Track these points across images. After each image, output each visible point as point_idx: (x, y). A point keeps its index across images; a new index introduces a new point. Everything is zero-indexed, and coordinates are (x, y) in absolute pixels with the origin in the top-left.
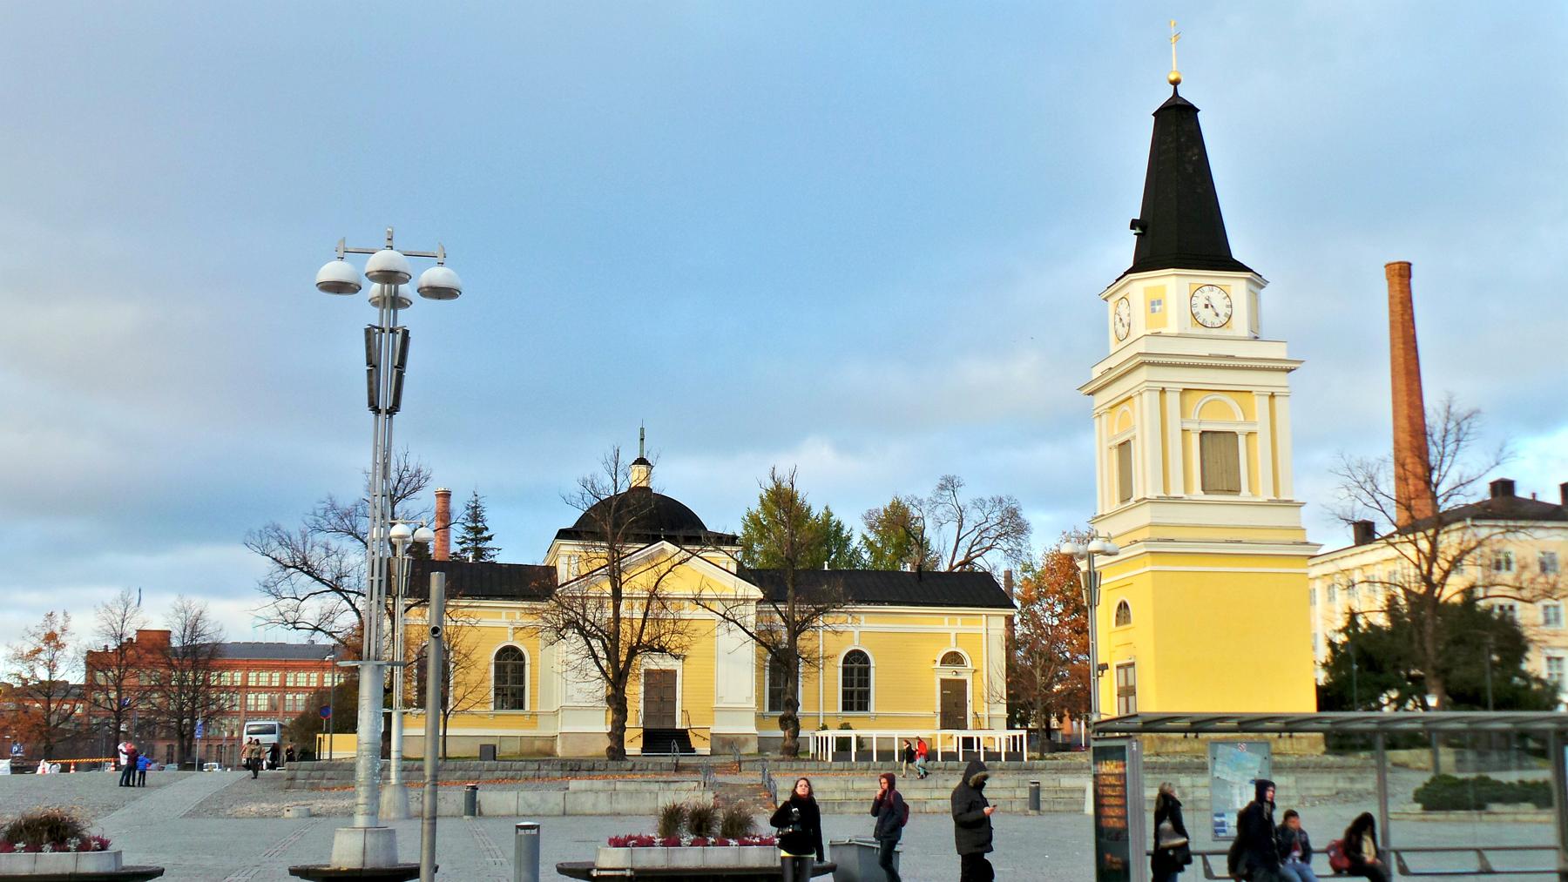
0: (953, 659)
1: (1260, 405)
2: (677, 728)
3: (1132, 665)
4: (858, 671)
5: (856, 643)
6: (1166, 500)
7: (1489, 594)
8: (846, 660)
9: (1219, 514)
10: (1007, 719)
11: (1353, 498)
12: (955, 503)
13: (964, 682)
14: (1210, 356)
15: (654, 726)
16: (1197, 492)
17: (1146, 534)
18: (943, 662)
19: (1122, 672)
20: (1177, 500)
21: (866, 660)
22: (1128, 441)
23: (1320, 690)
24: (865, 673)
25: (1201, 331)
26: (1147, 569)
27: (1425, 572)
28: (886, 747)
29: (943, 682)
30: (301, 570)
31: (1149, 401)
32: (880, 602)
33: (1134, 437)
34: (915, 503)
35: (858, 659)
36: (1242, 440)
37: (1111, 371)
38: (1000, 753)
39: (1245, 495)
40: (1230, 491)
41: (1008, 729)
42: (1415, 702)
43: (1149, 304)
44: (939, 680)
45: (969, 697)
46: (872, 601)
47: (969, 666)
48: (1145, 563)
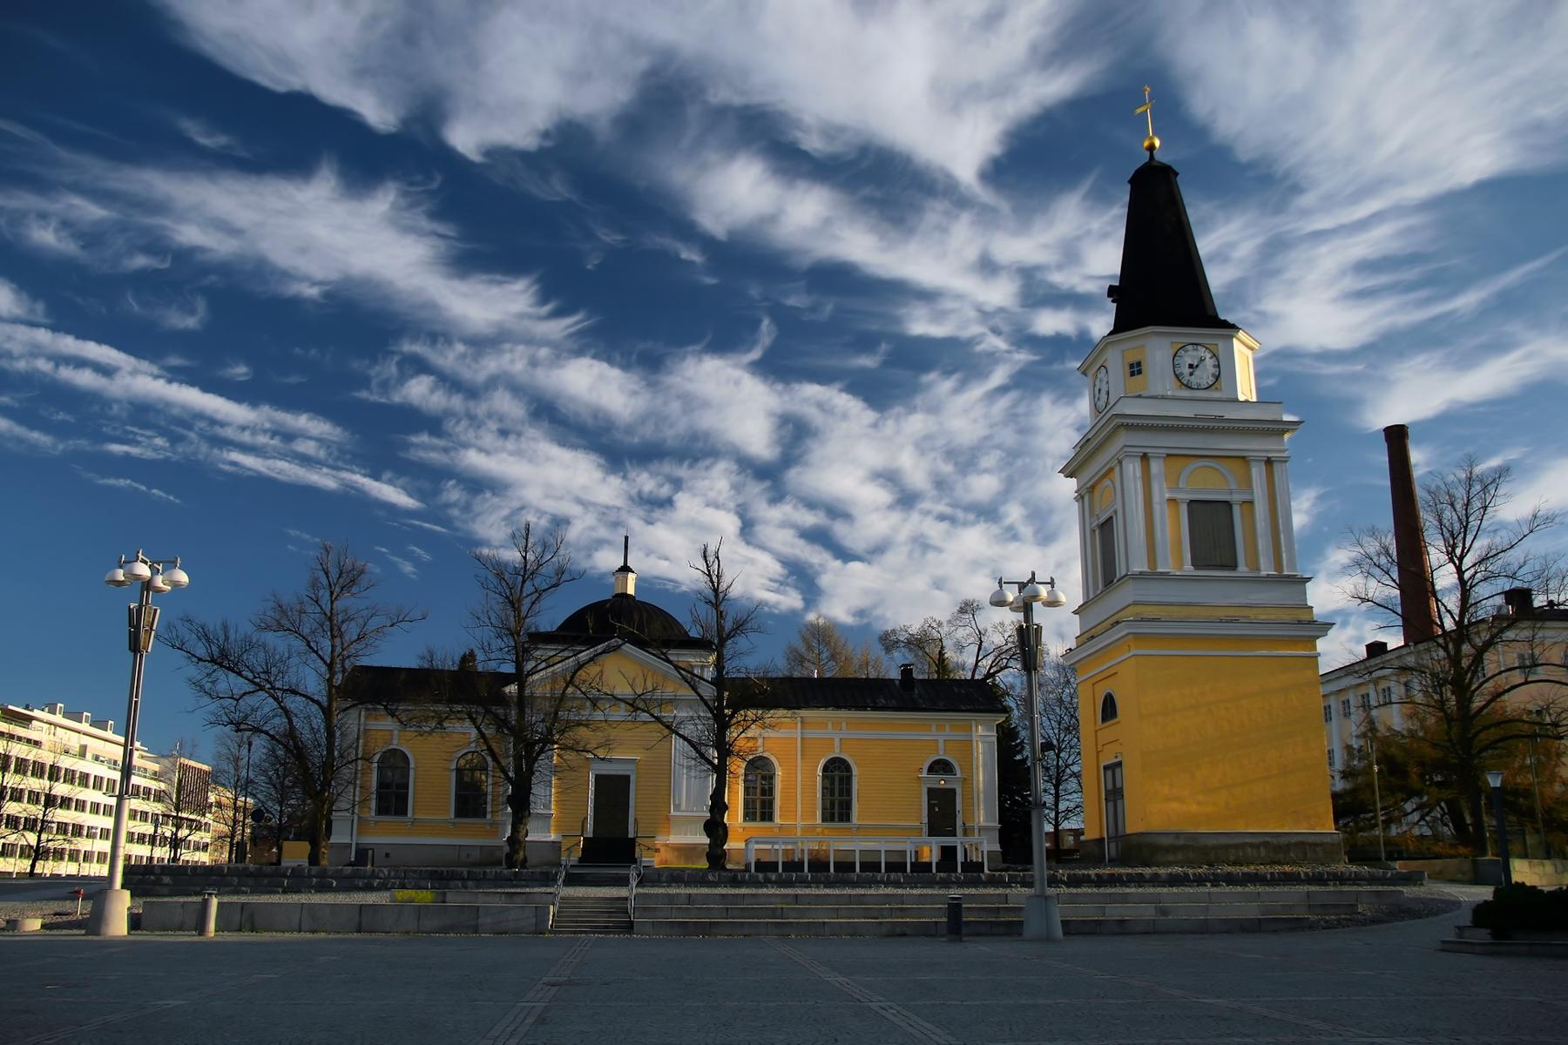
0: (940, 767)
1: (1257, 472)
2: (629, 837)
3: (1119, 764)
4: (840, 780)
5: (837, 750)
6: (1152, 576)
7: (1529, 679)
8: (825, 769)
9: (1218, 594)
10: (1000, 831)
11: (1366, 574)
12: (974, 627)
13: (953, 791)
14: (1194, 419)
15: (892, 860)
16: (1188, 568)
17: (1129, 614)
18: (931, 770)
19: (1109, 773)
20: (1165, 577)
21: (848, 768)
22: (1111, 517)
23: (1335, 796)
24: (847, 781)
25: (1186, 393)
26: (1131, 653)
27: (1452, 653)
28: (869, 859)
29: (930, 791)
30: (221, 665)
31: (1133, 469)
32: (861, 707)
33: (1116, 512)
34: (934, 625)
35: (840, 768)
36: (1237, 512)
37: (1090, 442)
38: (983, 863)
39: (1243, 569)
40: (1223, 567)
41: (625, 779)
42: (1442, 809)
43: (1127, 367)
44: (926, 790)
45: (959, 807)
46: (854, 707)
47: (959, 775)
48: (1129, 646)
